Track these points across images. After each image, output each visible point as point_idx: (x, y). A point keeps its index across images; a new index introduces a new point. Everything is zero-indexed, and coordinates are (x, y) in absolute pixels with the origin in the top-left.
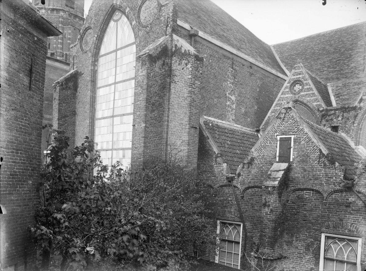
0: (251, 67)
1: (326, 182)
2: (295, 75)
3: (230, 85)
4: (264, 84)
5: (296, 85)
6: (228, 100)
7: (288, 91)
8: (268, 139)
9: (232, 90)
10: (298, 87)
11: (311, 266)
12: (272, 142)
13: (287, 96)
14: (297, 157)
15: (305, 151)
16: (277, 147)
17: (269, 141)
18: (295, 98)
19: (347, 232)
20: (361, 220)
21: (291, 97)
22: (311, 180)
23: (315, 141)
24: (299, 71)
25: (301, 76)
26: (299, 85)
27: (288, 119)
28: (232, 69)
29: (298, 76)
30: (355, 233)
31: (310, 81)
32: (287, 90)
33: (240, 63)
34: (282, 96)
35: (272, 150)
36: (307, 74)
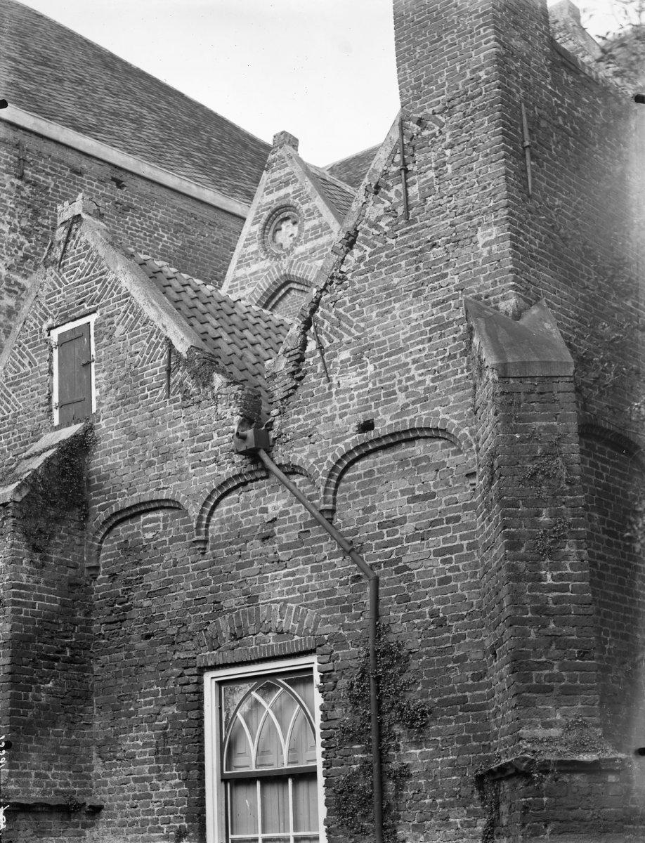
0: (119, 184)
1: (193, 459)
2: (272, 192)
3: (13, 236)
4: (195, 250)
5: (283, 226)
6: (10, 291)
7: (256, 252)
8: (24, 349)
9: (25, 257)
10: (287, 232)
11: (178, 825)
12: (37, 356)
13: (254, 268)
14: (108, 390)
15: (129, 359)
16: (50, 372)
17: (28, 354)
18: (279, 270)
19: (272, 643)
20: (310, 578)
21: (268, 269)
22: (151, 464)
23: (150, 312)
24: (283, 172)
25: (290, 189)
26: (289, 223)
27: (74, 260)
28: (17, 182)
29: (282, 192)
30: (296, 638)
31: (319, 202)
32: (254, 247)
33: (62, 162)
34: (240, 273)
35: (37, 388)
36: (307, 179)
